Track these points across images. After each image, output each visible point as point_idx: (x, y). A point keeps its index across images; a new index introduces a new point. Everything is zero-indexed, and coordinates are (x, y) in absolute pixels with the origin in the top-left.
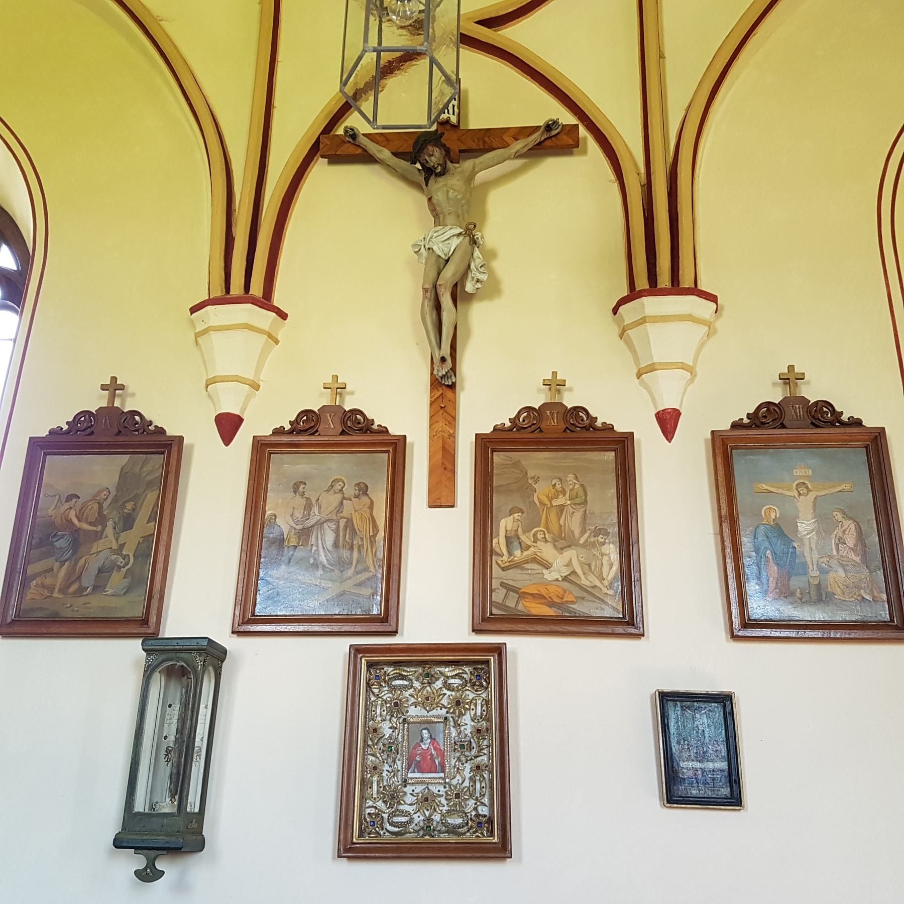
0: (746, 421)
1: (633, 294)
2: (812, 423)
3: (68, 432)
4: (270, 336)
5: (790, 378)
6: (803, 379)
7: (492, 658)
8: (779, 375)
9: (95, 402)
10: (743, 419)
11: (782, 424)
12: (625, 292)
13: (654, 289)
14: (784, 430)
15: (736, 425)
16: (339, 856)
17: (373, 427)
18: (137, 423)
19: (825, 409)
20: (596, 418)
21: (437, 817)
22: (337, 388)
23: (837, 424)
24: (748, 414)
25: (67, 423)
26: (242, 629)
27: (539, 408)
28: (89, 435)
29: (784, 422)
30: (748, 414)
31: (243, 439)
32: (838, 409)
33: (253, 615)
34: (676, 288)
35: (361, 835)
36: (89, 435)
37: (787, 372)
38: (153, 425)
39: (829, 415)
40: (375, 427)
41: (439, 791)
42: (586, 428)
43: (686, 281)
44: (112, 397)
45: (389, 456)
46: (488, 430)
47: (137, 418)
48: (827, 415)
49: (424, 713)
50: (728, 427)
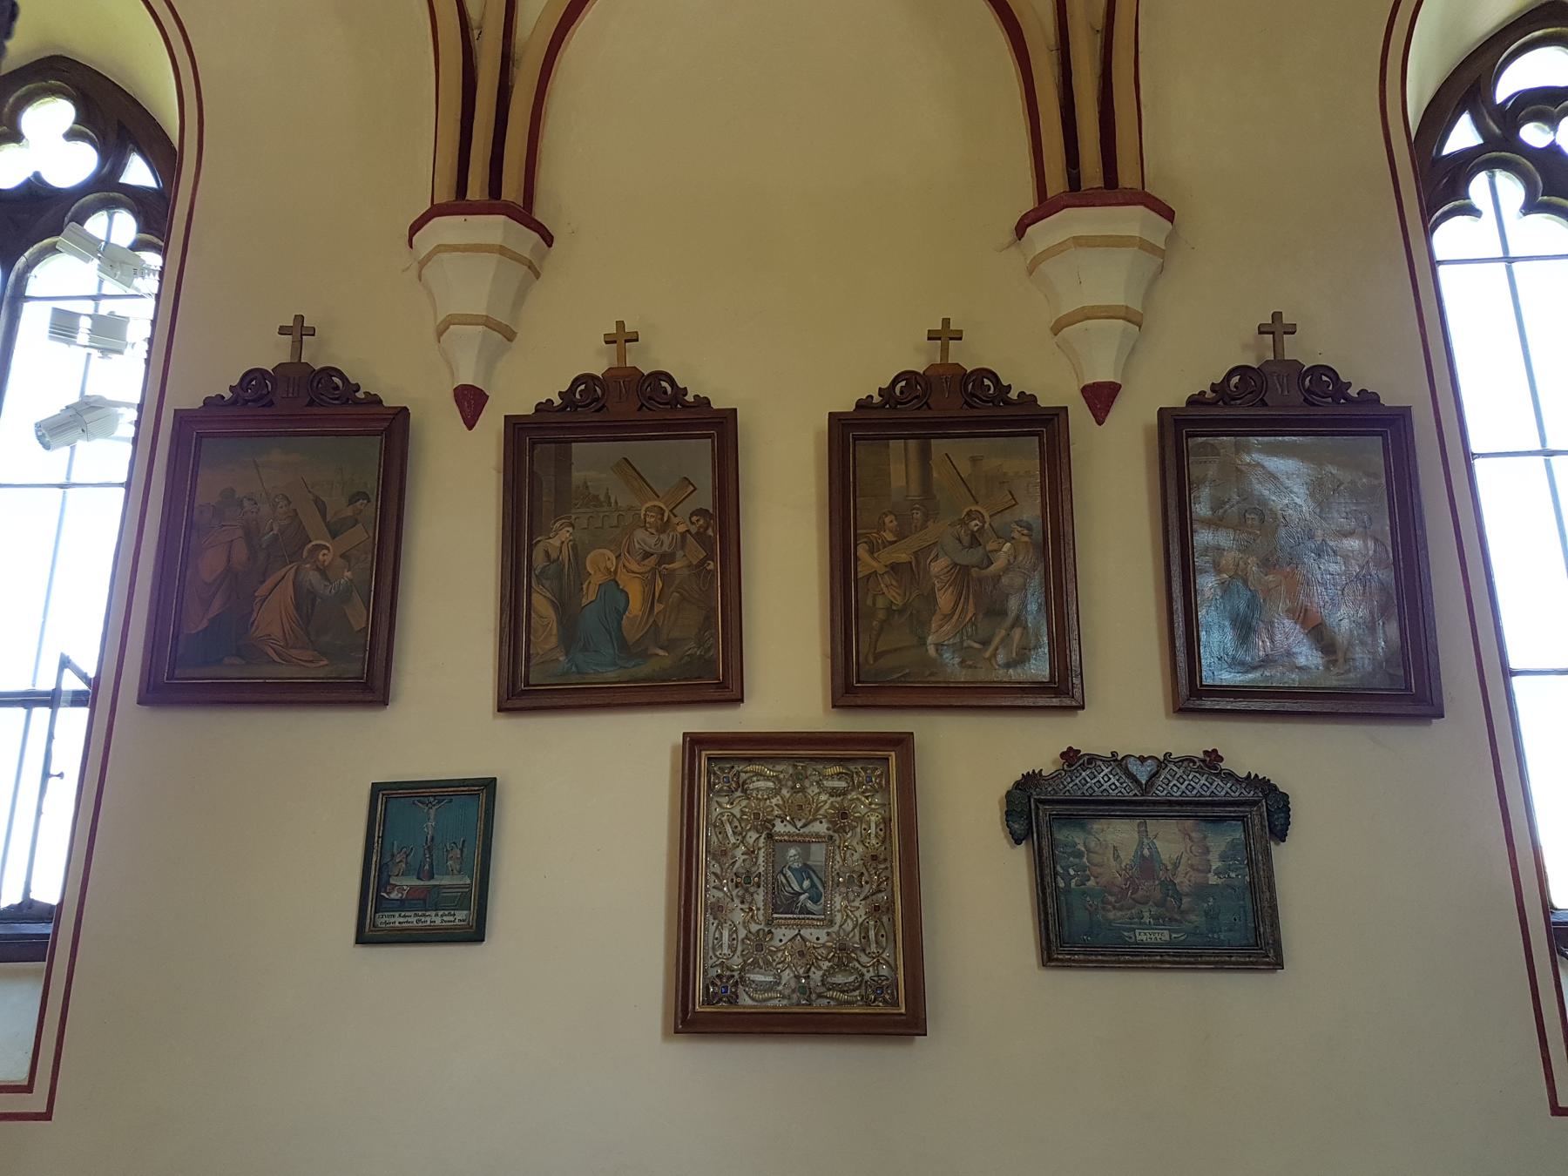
0: (1209, 395)
1: (1045, 207)
2: (966, 402)
3: (562, 409)
4: (531, 266)
5: (1277, 328)
6: (1293, 333)
7: (893, 753)
8: (1259, 327)
9: (271, 354)
10: (1205, 392)
11: (1262, 400)
12: (1028, 202)
13: (1076, 194)
14: (1265, 408)
15: (1193, 401)
16: (677, 1032)
17: (686, 398)
18: (337, 388)
19: (1324, 378)
20: (1010, 386)
21: (816, 975)
22: (602, 528)
23: (1342, 401)
24: (1213, 384)
25: (231, 388)
26: (509, 705)
27: (924, 372)
28: (598, 411)
29: (1265, 398)
30: (1213, 384)
31: (1080, 415)
32: (1343, 379)
33: (527, 684)
34: (1111, 190)
35: (708, 1000)
36: (598, 411)
37: (1270, 322)
38: (362, 390)
39: (1331, 388)
40: (690, 398)
41: (818, 939)
42: (992, 400)
43: (1127, 178)
44: (298, 347)
45: (713, 442)
46: (848, 406)
47: (336, 379)
48: (1329, 387)
49: (792, 830)
50: (851, 408)
